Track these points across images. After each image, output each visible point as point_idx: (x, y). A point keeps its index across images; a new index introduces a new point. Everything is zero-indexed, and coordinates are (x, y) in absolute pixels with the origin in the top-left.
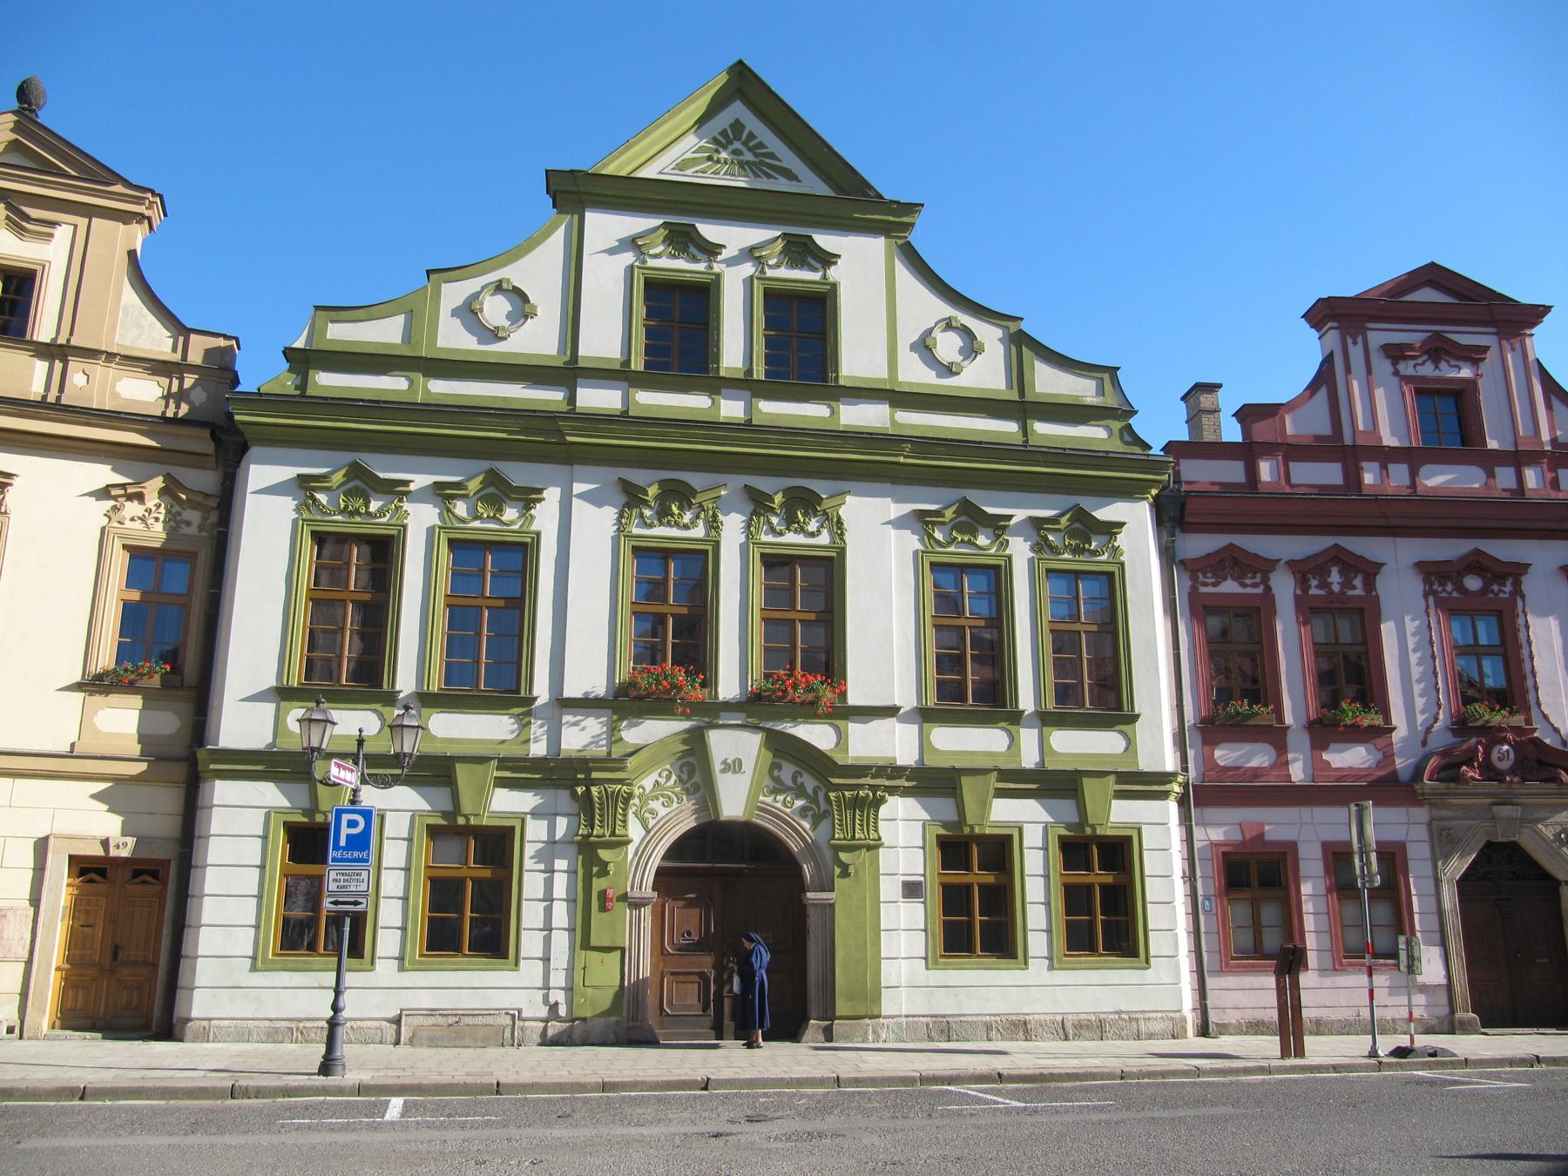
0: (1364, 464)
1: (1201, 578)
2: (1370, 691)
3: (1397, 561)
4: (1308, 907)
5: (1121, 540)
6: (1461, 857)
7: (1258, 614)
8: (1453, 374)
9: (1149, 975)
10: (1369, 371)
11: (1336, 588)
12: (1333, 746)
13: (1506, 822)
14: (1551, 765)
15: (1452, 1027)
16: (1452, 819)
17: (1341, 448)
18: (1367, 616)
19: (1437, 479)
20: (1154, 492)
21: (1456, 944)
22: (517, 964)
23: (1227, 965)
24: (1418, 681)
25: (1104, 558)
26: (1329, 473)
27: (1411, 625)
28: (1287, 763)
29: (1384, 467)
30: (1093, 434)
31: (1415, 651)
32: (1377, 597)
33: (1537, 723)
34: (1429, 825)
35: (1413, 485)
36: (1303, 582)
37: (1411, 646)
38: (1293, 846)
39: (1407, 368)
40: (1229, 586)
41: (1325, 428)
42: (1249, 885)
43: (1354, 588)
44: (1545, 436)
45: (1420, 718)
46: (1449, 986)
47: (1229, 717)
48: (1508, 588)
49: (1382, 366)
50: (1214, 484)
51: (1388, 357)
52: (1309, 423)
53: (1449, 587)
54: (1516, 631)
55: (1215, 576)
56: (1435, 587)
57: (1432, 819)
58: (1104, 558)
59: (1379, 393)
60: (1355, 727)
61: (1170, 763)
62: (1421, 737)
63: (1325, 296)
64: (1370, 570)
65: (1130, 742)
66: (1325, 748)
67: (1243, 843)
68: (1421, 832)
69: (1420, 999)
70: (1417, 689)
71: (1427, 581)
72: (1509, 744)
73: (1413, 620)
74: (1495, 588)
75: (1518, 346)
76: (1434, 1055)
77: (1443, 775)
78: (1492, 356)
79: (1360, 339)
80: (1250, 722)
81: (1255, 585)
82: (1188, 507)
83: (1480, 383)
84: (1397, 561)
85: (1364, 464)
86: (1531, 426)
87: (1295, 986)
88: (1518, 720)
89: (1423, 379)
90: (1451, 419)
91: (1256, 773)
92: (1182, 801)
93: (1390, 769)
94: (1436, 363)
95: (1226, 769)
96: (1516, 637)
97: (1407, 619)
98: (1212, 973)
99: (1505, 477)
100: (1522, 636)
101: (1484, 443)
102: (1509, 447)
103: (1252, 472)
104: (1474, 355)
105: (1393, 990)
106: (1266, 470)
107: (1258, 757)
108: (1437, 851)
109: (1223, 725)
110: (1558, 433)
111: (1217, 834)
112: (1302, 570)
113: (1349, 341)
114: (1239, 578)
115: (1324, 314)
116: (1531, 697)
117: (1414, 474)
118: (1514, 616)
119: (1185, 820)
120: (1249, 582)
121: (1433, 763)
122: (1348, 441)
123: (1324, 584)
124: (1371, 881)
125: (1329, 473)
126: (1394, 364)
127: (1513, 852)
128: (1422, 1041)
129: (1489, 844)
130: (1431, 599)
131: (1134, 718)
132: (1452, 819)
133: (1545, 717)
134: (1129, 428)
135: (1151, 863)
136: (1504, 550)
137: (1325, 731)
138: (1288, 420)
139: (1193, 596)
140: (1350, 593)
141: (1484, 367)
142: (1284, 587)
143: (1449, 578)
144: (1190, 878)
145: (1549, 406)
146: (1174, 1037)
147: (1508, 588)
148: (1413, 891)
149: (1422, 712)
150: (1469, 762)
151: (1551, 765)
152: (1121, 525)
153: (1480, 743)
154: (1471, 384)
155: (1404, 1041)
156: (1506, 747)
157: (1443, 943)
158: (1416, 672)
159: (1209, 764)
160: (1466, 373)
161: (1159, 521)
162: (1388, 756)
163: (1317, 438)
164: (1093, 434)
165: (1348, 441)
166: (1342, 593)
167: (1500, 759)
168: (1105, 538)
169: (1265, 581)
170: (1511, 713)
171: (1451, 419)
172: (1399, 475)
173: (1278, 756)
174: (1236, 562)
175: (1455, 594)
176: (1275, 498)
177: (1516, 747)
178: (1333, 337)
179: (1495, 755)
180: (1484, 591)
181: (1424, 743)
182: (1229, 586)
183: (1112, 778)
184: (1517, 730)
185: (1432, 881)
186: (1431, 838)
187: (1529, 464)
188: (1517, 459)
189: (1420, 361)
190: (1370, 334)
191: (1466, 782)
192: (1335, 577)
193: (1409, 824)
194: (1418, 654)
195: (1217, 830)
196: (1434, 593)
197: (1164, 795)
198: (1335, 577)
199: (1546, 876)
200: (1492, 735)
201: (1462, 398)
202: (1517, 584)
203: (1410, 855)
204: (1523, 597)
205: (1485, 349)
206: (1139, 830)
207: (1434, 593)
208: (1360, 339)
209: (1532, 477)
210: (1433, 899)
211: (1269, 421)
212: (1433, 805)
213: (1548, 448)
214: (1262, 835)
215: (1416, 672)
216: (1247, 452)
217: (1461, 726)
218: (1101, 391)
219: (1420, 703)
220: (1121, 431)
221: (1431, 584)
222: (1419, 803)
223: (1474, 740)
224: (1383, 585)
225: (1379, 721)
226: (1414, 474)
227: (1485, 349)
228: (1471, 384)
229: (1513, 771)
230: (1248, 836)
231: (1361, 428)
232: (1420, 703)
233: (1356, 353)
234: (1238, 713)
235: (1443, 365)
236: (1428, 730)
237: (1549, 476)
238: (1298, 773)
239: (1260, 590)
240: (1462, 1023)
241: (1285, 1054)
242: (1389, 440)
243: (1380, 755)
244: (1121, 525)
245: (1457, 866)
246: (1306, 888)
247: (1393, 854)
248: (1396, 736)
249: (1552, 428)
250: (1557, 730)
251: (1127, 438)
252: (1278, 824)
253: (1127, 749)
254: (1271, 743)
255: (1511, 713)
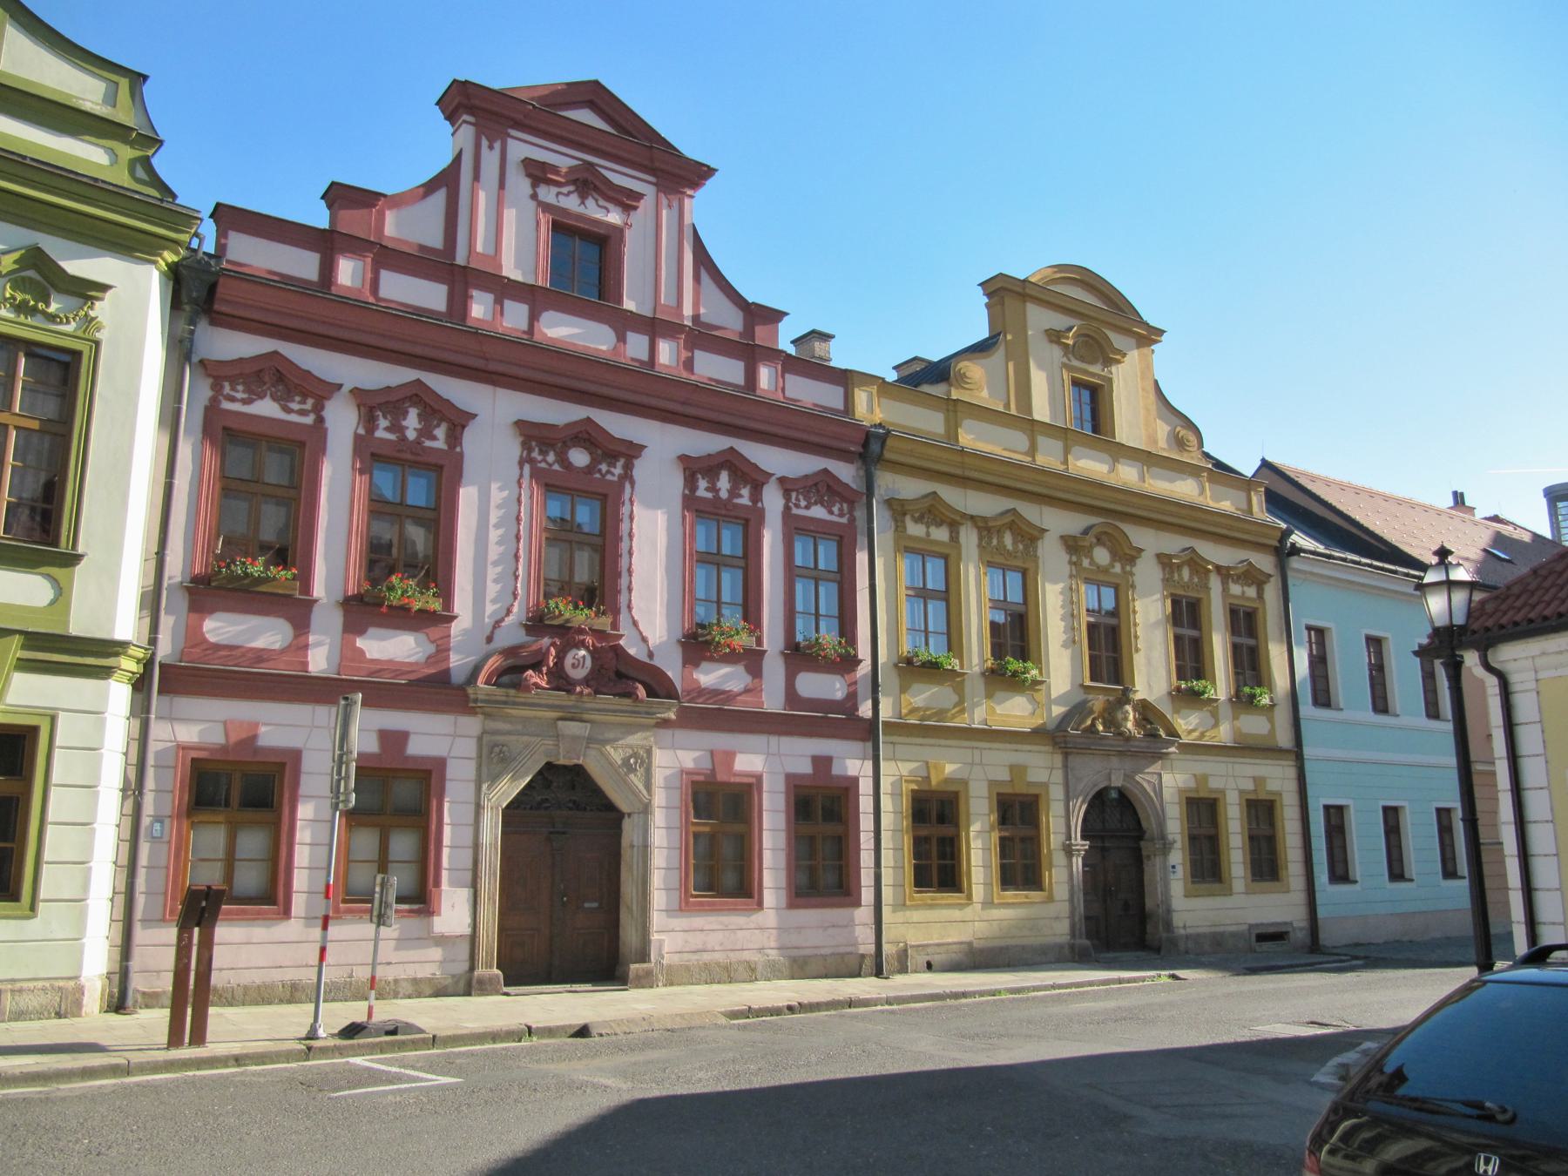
0: (475, 293)
1: (227, 389)
2: (435, 571)
3: (495, 416)
4: (303, 835)
5: (101, 309)
6: (514, 779)
7: (302, 450)
8: (599, 215)
9: (32, 927)
10: (502, 185)
11: (411, 435)
12: (372, 631)
13: (568, 743)
14: (628, 678)
15: (469, 986)
16: (509, 733)
17: (462, 278)
18: (445, 473)
19: (560, 329)
20: (170, 257)
21: (490, 885)
22: (33, 907)
23: (687, 903)
24: (495, 564)
25: (70, 328)
26: (430, 295)
27: (497, 495)
28: (306, 647)
29: (499, 301)
30: (87, 155)
31: (497, 526)
32: (461, 455)
33: (625, 628)
34: (480, 739)
35: (531, 331)
36: (369, 421)
37: (493, 519)
38: (296, 755)
39: (548, 194)
40: (267, 408)
41: (435, 240)
42: (227, 804)
43: (434, 438)
44: (688, 311)
45: (490, 608)
46: (473, 938)
47: (234, 578)
48: (618, 471)
49: (519, 184)
50: (271, 272)
51: (529, 175)
52: (414, 227)
53: (551, 457)
54: (618, 520)
55: (248, 390)
56: (535, 454)
57: (484, 732)
58: (70, 328)
59: (510, 215)
60: (404, 609)
61: (126, 624)
62: (488, 632)
63: (462, 79)
64: (458, 421)
65: (61, 593)
66: (361, 632)
67: (224, 749)
68: (468, 747)
69: (436, 953)
70: (492, 572)
71: (526, 445)
72: (587, 648)
73: (501, 489)
74: (604, 467)
75: (675, 204)
76: (394, 1032)
77: (505, 679)
78: (646, 205)
79: (497, 145)
80: (263, 588)
81: (302, 413)
82: (220, 289)
83: (627, 233)
84: (495, 416)
85: (475, 293)
86: (674, 291)
87: (207, 944)
88: (604, 623)
89: (565, 212)
90: (585, 264)
91: (260, 656)
92: (140, 685)
93: (443, 666)
94: (583, 198)
95: (217, 647)
96: (617, 529)
97: (494, 486)
98: (147, 922)
99: (636, 346)
100: (624, 527)
101: (620, 300)
102: (647, 312)
103: (328, 269)
104: (627, 201)
105: (403, 942)
106: (348, 272)
107: (264, 634)
108: (484, 769)
109: (218, 588)
110: (702, 311)
111: (189, 734)
112: (370, 404)
113: (485, 143)
114: (283, 400)
115: (462, 101)
116: (623, 599)
117: (533, 318)
118: (618, 503)
119: (141, 709)
120: (295, 406)
121: (493, 663)
122: (460, 259)
123: (396, 427)
124: (347, 801)
125: (430, 295)
126: (534, 185)
127: (577, 775)
128: (387, 1011)
129: (548, 764)
130: (527, 468)
131: (72, 560)
132: (509, 733)
133: (635, 624)
134: (146, 163)
135: (64, 767)
136: (618, 425)
137: (364, 610)
138: (390, 217)
139: (212, 413)
140: (428, 443)
141: (635, 217)
142: (342, 421)
143: (552, 446)
144: (133, 790)
145: (697, 279)
146: (59, 1015)
147: (618, 471)
148: (447, 819)
149: (494, 601)
150: (536, 666)
151: (628, 678)
152: (104, 288)
153: (553, 644)
154: (617, 233)
155: (354, 1012)
156: (583, 652)
157: (474, 885)
158: (494, 552)
159: (193, 637)
160: (614, 217)
161: (176, 303)
162: (442, 651)
163: (422, 248)
164: (87, 155)
165: (460, 259)
166: (418, 442)
167: (573, 666)
168: (74, 301)
169: (318, 409)
170: (597, 614)
171: (585, 264)
172: (515, 317)
173: (296, 637)
174: (280, 378)
175: (556, 467)
176: (348, 302)
177: (595, 653)
178: (467, 132)
179: (569, 661)
180: (590, 470)
181: (489, 639)
182: (267, 408)
183: (17, 640)
184: (599, 634)
185: (472, 807)
186: (480, 756)
187: (664, 336)
188: (654, 327)
189: (565, 190)
190: (510, 141)
191: (527, 689)
192: (412, 422)
193: (455, 736)
194: (500, 531)
195: (196, 726)
196: (531, 461)
197: (105, 673)
198: (412, 422)
199: (610, 807)
200: (567, 636)
201: (605, 243)
202: (628, 467)
203: (450, 773)
204: (633, 484)
205: (639, 196)
206: (53, 719)
207: (531, 461)
208: (497, 145)
209: (667, 353)
210: (471, 830)
211: (364, 211)
212: (487, 715)
213: (688, 323)
214: (255, 737)
215: (494, 552)
216: (327, 243)
217: (537, 623)
218: (111, 99)
219: (492, 589)
220: (132, 163)
221: (530, 450)
222: (472, 712)
223: (546, 641)
224: (472, 441)
225: (436, 605)
226: (533, 318)
227: (639, 196)
228: (617, 233)
229: (586, 681)
230: (234, 738)
231: (479, 248)
232: (492, 589)
233: (490, 160)
234: (246, 575)
235: (590, 202)
236: (497, 624)
237: (685, 354)
238: (319, 661)
239: (309, 420)
240: (481, 982)
241: (175, 1039)
242: (511, 269)
243: (431, 649)
244: (104, 288)
245: (508, 789)
246: (305, 811)
247: (429, 772)
248: (456, 628)
249: (696, 304)
250: (644, 640)
251: (140, 173)
252: (278, 725)
253: (52, 603)
254: (288, 619)
255: (597, 614)
